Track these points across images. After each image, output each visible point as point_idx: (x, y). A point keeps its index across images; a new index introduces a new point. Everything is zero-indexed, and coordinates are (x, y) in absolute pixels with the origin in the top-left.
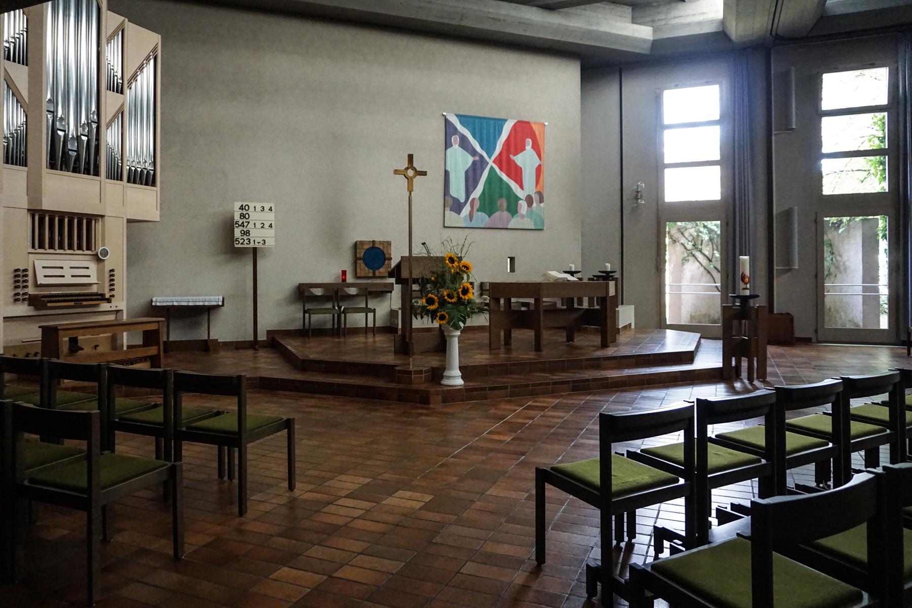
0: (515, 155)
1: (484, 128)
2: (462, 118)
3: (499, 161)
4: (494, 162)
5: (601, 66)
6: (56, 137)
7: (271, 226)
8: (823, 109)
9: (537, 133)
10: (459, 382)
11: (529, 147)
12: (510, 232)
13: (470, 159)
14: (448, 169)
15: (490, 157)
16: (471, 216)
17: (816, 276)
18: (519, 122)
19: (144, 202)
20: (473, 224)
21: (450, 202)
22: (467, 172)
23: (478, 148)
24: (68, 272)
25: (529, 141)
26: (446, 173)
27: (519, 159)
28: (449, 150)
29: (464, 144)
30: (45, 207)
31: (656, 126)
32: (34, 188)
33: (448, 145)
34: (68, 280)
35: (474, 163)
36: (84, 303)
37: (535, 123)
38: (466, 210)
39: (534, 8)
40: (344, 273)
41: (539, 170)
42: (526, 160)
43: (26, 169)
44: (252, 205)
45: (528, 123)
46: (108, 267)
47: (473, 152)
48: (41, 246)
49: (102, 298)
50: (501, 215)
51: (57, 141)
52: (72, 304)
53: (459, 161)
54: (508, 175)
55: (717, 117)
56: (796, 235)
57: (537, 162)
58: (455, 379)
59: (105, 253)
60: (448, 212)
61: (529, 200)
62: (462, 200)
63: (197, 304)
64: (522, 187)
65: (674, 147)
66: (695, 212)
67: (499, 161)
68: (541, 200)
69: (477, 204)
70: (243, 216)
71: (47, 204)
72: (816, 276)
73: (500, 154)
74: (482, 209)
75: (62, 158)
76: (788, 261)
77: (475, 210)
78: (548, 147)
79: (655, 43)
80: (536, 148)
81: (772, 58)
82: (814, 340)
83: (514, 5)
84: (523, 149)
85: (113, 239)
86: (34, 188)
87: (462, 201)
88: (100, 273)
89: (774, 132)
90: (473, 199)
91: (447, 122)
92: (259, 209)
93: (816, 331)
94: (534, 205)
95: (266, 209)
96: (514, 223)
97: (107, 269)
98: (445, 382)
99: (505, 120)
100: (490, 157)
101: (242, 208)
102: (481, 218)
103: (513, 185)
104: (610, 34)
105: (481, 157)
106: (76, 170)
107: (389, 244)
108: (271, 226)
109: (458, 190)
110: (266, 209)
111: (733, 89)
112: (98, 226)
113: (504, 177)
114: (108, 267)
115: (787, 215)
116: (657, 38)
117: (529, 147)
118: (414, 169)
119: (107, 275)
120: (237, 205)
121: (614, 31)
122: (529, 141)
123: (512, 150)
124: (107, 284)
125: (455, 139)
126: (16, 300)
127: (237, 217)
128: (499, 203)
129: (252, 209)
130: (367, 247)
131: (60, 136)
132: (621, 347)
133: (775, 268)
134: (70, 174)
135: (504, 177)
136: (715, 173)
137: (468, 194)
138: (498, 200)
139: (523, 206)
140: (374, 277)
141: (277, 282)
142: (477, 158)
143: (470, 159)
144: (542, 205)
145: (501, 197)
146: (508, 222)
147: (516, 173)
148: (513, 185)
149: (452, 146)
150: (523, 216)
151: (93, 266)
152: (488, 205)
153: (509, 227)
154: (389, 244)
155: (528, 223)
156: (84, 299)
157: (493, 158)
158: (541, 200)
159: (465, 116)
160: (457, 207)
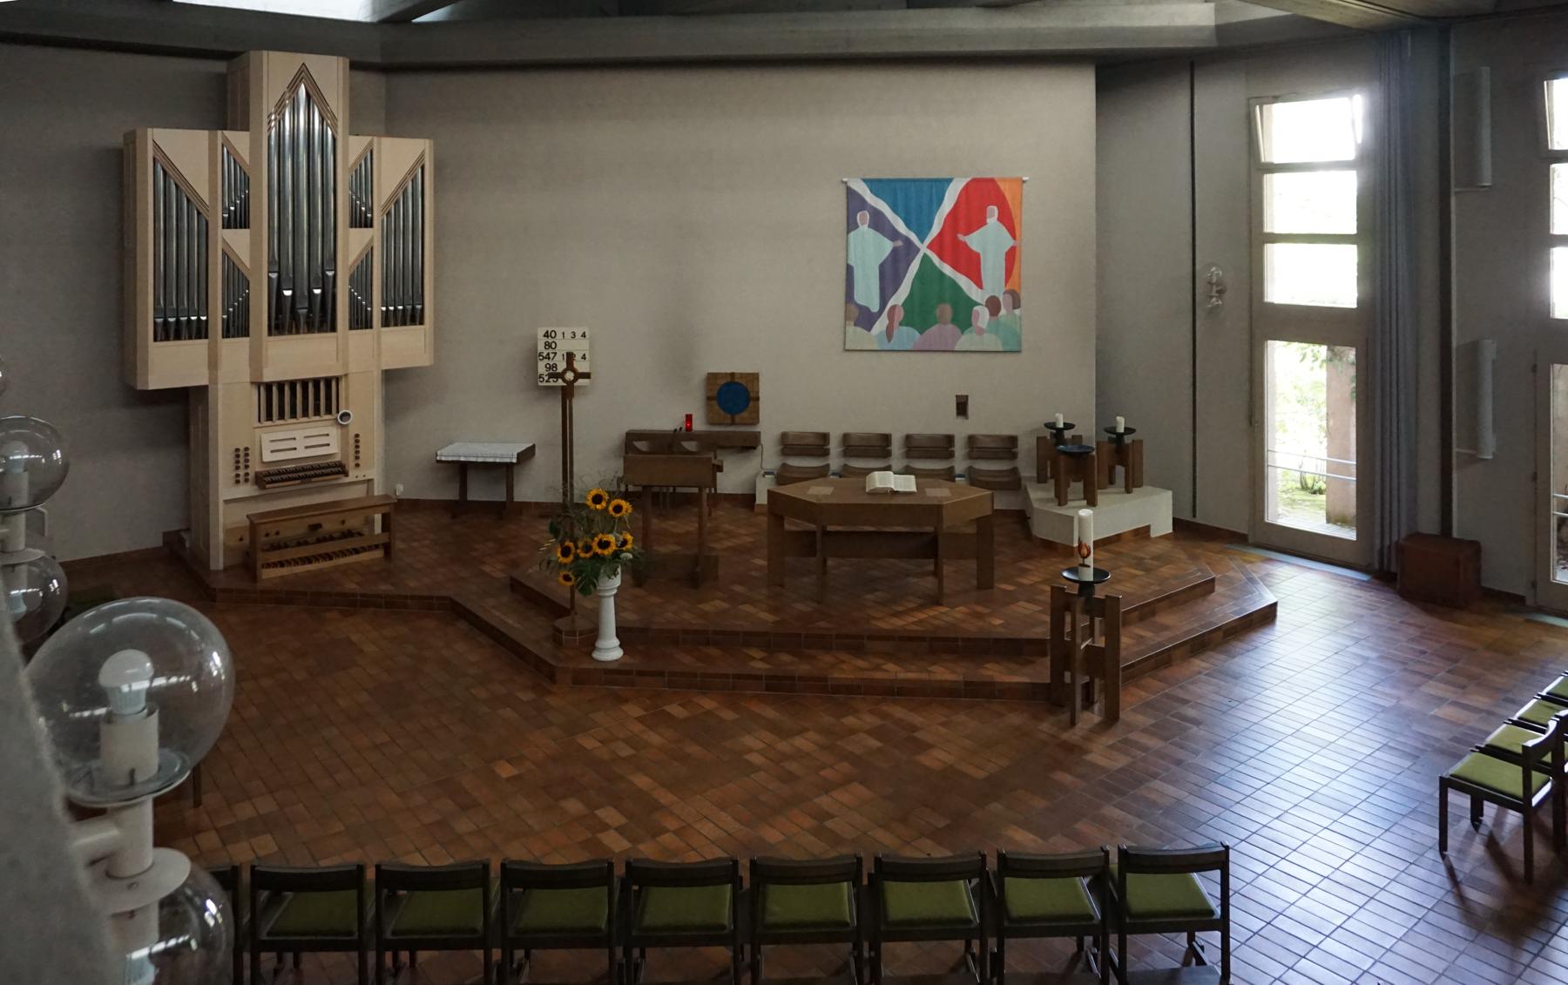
0: (968, 231)
1: (914, 196)
2: (876, 185)
3: (937, 246)
4: (918, 250)
5: (1128, 72)
7: (584, 357)
8: (1557, 147)
9: (1008, 195)
10: (617, 654)
11: (992, 219)
12: (959, 356)
13: (888, 246)
14: (851, 263)
15: (922, 241)
16: (889, 332)
17: (1535, 477)
18: (975, 181)
19: (405, 346)
20: (894, 345)
21: (855, 312)
22: (882, 266)
23: (901, 227)
24: (300, 444)
25: (993, 210)
26: (849, 270)
27: (974, 241)
28: (852, 234)
29: (879, 223)
30: (266, 379)
31: (1255, 169)
32: (256, 360)
33: (851, 225)
35: (895, 251)
37: (1004, 180)
38: (881, 325)
39: (973, 10)
40: (689, 418)
41: (1011, 256)
42: (989, 240)
44: (559, 331)
45: (992, 181)
46: (352, 431)
47: (894, 235)
48: (269, 417)
49: (340, 469)
50: (942, 331)
53: (870, 249)
54: (955, 267)
55: (1350, 154)
57: (1009, 242)
58: (610, 650)
59: (346, 416)
60: (851, 329)
61: (993, 305)
62: (875, 308)
64: (979, 284)
65: (1284, 205)
66: (1307, 324)
67: (937, 246)
68: (1016, 304)
69: (900, 315)
70: (548, 345)
71: (269, 376)
72: (1535, 477)
73: (940, 234)
74: (906, 322)
76: (1474, 440)
77: (896, 323)
78: (1029, 216)
79: (1220, 30)
80: (1007, 219)
81: (1452, 49)
82: (1529, 602)
83: (935, 12)
84: (983, 223)
85: (363, 401)
86: (256, 360)
87: (875, 308)
88: (344, 438)
89: (1453, 190)
90: (894, 307)
91: (851, 194)
92: (568, 335)
93: (1534, 585)
94: (1003, 312)
95: (578, 335)
96: (966, 341)
98: (596, 655)
99: (949, 181)
100: (922, 241)
101: (546, 335)
102: (907, 335)
103: (963, 282)
104: (1124, 29)
105: (907, 241)
107: (754, 377)
108: (584, 357)
109: (867, 294)
110: (578, 335)
111: (1388, 99)
112: (342, 384)
113: (947, 270)
114: (352, 431)
115: (1473, 349)
116: (1222, 21)
117: (992, 219)
118: (574, 371)
119: (352, 441)
120: (541, 332)
121: (1137, 23)
122: (993, 210)
123: (962, 224)
125: (863, 217)
126: (238, 482)
127: (541, 348)
128: (937, 311)
129: (559, 336)
130: (722, 382)
133: (1455, 450)
135: (947, 270)
136: (1349, 256)
137: (884, 301)
138: (935, 309)
139: (983, 315)
140: (733, 423)
141: (601, 426)
142: (900, 243)
143: (888, 246)
144: (1017, 312)
145: (941, 300)
146: (954, 343)
147: (970, 265)
148: (963, 282)
149: (857, 227)
150: (981, 332)
151: (334, 432)
152: (919, 314)
153: (957, 348)
154: (754, 377)
155: (991, 342)
157: (928, 240)
158: (1016, 304)
159: (880, 181)
160: (866, 319)
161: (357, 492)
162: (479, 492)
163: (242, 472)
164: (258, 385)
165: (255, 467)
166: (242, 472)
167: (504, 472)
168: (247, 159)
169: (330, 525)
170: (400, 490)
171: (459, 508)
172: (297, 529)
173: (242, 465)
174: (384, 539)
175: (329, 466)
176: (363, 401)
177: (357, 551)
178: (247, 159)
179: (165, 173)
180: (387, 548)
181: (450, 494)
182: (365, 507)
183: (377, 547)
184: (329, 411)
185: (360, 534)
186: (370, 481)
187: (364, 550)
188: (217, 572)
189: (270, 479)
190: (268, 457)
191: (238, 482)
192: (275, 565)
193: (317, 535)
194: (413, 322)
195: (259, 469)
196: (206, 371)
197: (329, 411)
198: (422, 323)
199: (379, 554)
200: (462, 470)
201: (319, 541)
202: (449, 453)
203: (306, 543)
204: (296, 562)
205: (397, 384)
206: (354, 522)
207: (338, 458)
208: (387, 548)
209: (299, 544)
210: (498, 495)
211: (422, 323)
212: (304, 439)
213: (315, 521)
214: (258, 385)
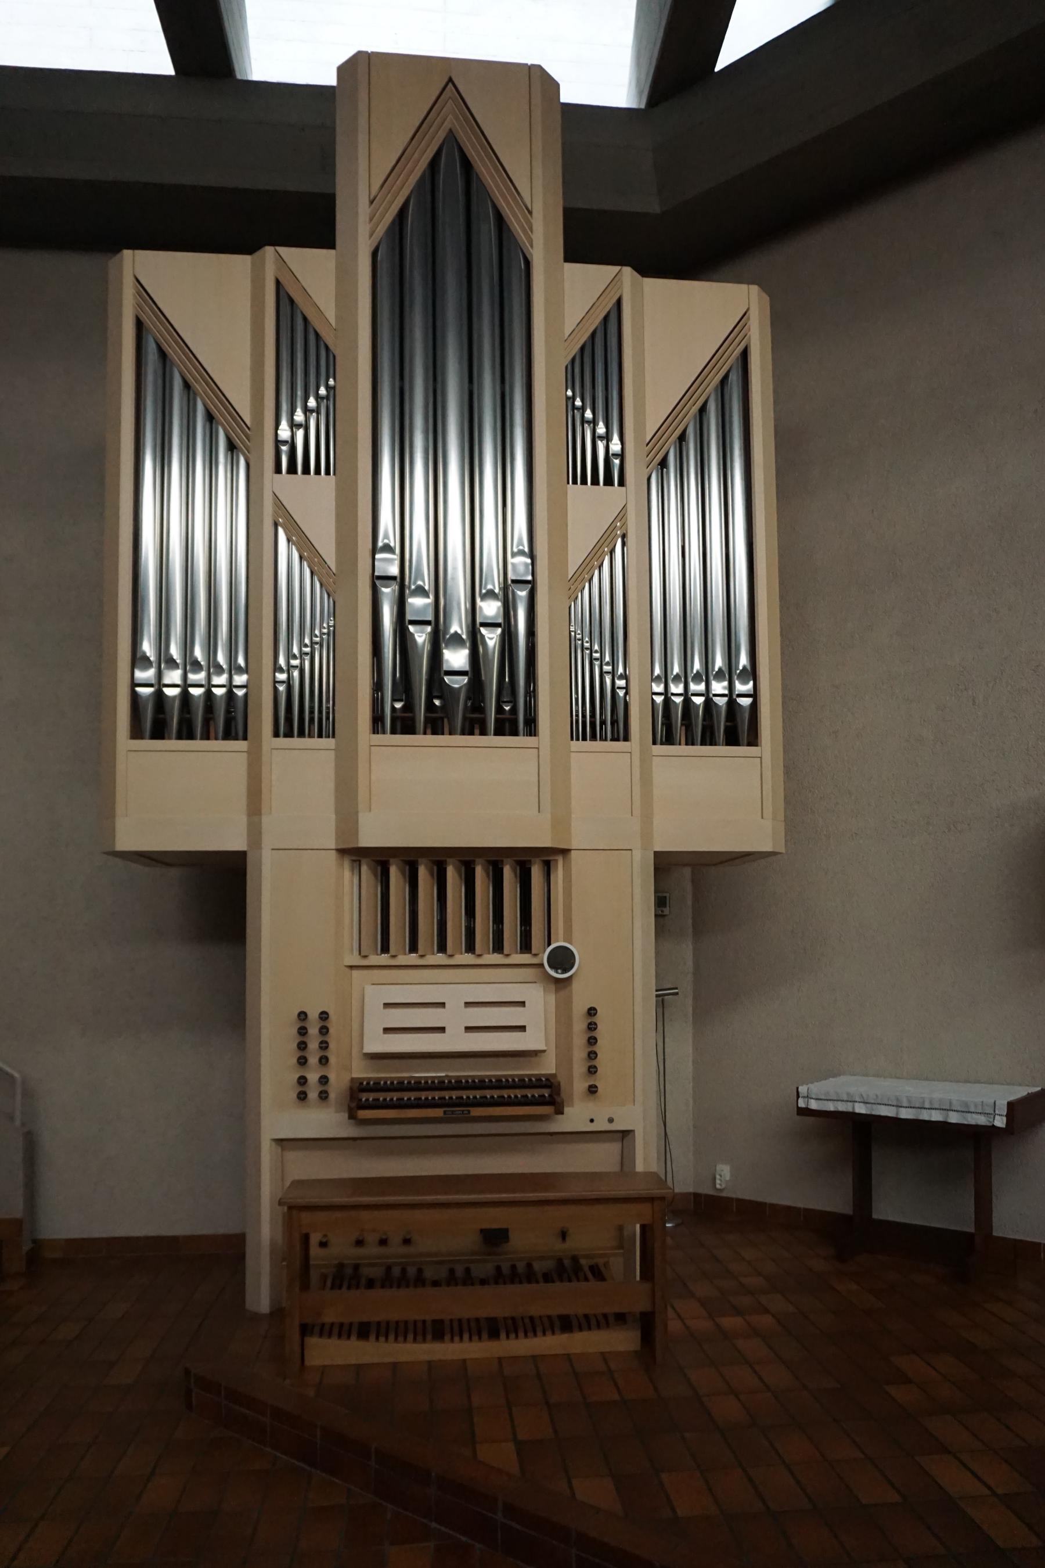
6: (672, 706)
24: (454, 1018)
34: (455, 1041)
36: (477, 1112)
43: (330, 742)
49: (548, 1094)
51: (673, 711)
52: (439, 1112)
56: (517, 1195)
63: (925, 1116)
71: (372, 835)
75: (423, 703)
85: (606, 914)
97: (579, 1008)
106: (474, 725)
114: (581, 997)
119: (579, 1026)
124: (579, 1054)
131: (697, 707)
132: (580, 836)
134: (492, 740)
151: (538, 1000)
156: (515, 1095)
161: (599, 1159)
162: (901, 1201)
163: (313, 1077)
164: (354, 855)
165: (347, 1069)
166: (313, 1077)
167: (962, 1150)
168: (331, 314)
169: (531, 1238)
170: (724, 1177)
171: (851, 1235)
172: (452, 1237)
173: (313, 1060)
174: (642, 1305)
175: (522, 1083)
176: (606, 914)
177: (566, 1324)
178: (331, 314)
179: (163, 355)
180: (647, 1325)
181: (831, 1197)
182: (595, 1200)
183: (621, 1318)
184: (526, 946)
185: (597, 1273)
186: (626, 1135)
187: (588, 1322)
188: (256, 1317)
189: (395, 1097)
190: (377, 1043)
191: (302, 1096)
192: (343, 1331)
193: (504, 1262)
194: (732, 739)
195: (361, 1071)
196: (242, 820)
197: (526, 946)
198: (753, 740)
199: (622, 1341)
200: (859, 1138)
201: (498, 1277)
202: (827, 1094)
203: (468, 1280)
204: (402, 1330)
205: (692, 888)
206: (590, 1238)
207: (548, 1067)
208: (647, 1325)
209: (452, 1279)
210: (953, 1214)
211: (753, 740)
212: (462, 1008)
213: (494, 1218)
214: (354, 855)
